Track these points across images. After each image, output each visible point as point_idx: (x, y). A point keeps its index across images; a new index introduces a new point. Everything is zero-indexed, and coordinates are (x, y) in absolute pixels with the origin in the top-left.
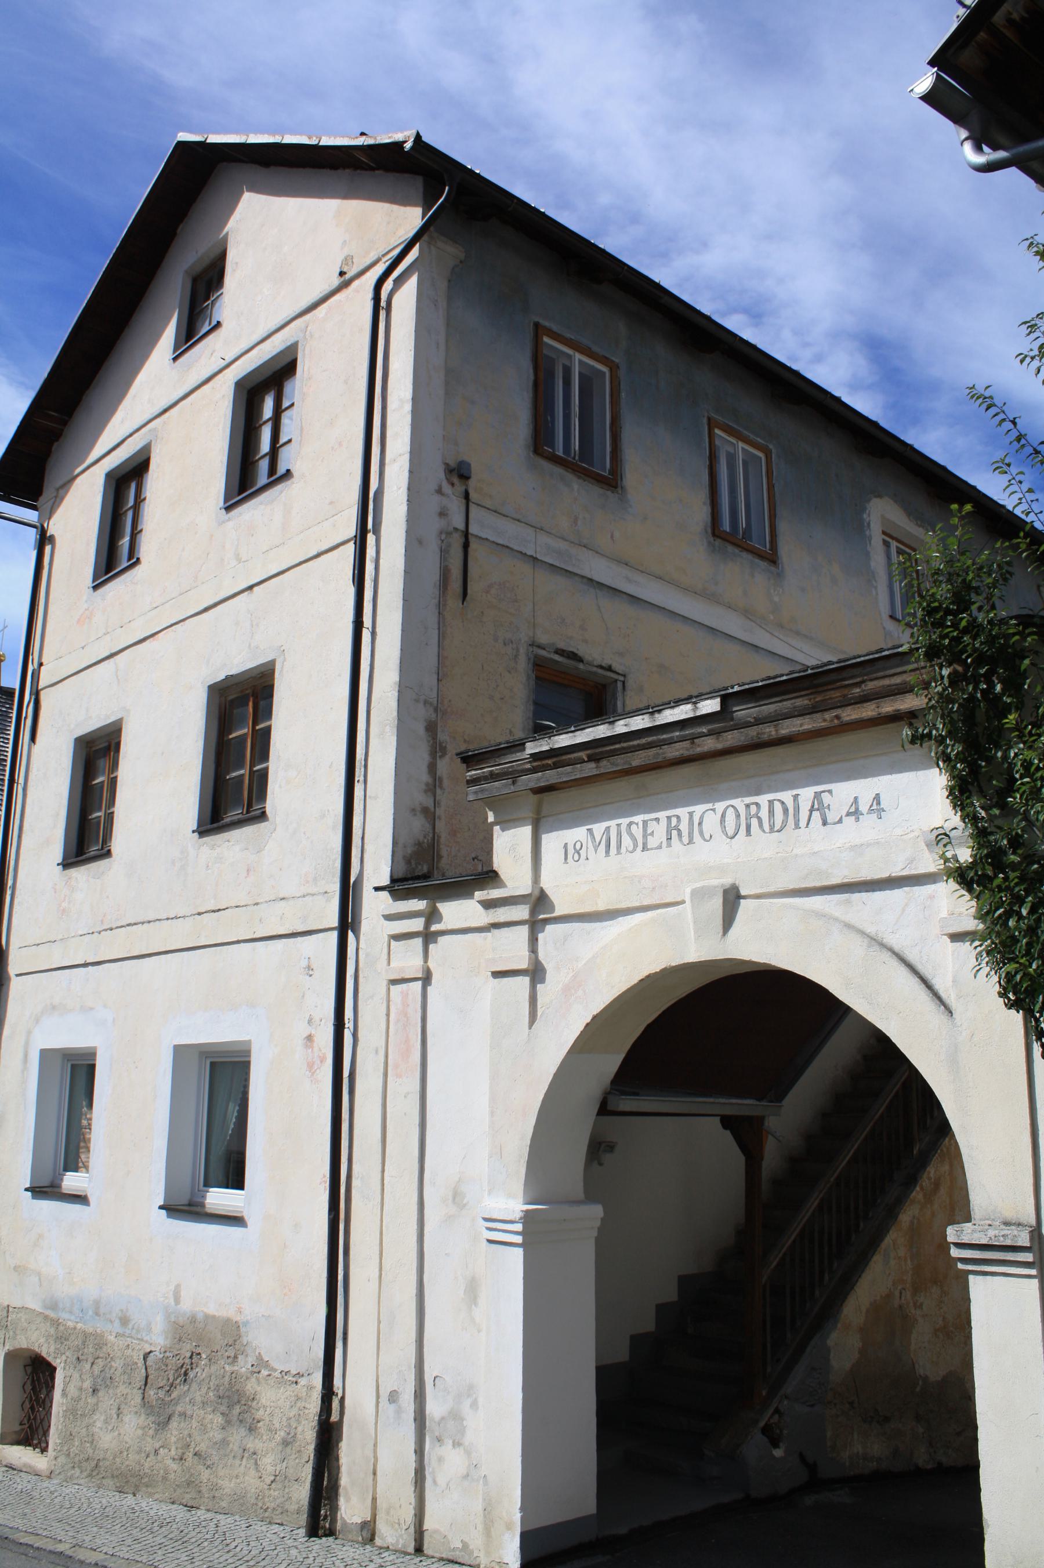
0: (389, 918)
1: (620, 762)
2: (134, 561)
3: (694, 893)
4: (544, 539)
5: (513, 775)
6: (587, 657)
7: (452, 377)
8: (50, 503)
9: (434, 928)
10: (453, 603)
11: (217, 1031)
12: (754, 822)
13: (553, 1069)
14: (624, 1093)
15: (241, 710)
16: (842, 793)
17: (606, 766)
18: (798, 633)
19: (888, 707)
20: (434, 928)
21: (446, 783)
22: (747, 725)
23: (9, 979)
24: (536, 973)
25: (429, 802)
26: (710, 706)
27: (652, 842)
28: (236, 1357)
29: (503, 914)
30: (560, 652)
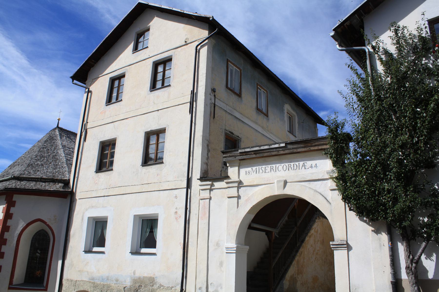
0: (200, 185)
1: (261, 155)
2: (118, 100)
3: (277, 181)
4: (228, 107)
5: (235, 156)
6: (235, 134)
7: (213, 69)
8: (90, 83)
9: (212, 188)
10: (212, 119)
11: (147, 211)
12: (290, 168)
13: (243, 216)
14: (254, 223)
15: (153, 138)
16: (309, 163)
17: (258, 155)
18: (271, 133)
19: (320, 147)
20: (212, 188)
21: (210, 158)
22: (290, 149)
23: (76, 200)
24: (239, 197)
25: (207, 162)
26: (283, 145)
27: (267, 171)
28: (153, 285)
29: (231, 185)
30: (230, 132)
